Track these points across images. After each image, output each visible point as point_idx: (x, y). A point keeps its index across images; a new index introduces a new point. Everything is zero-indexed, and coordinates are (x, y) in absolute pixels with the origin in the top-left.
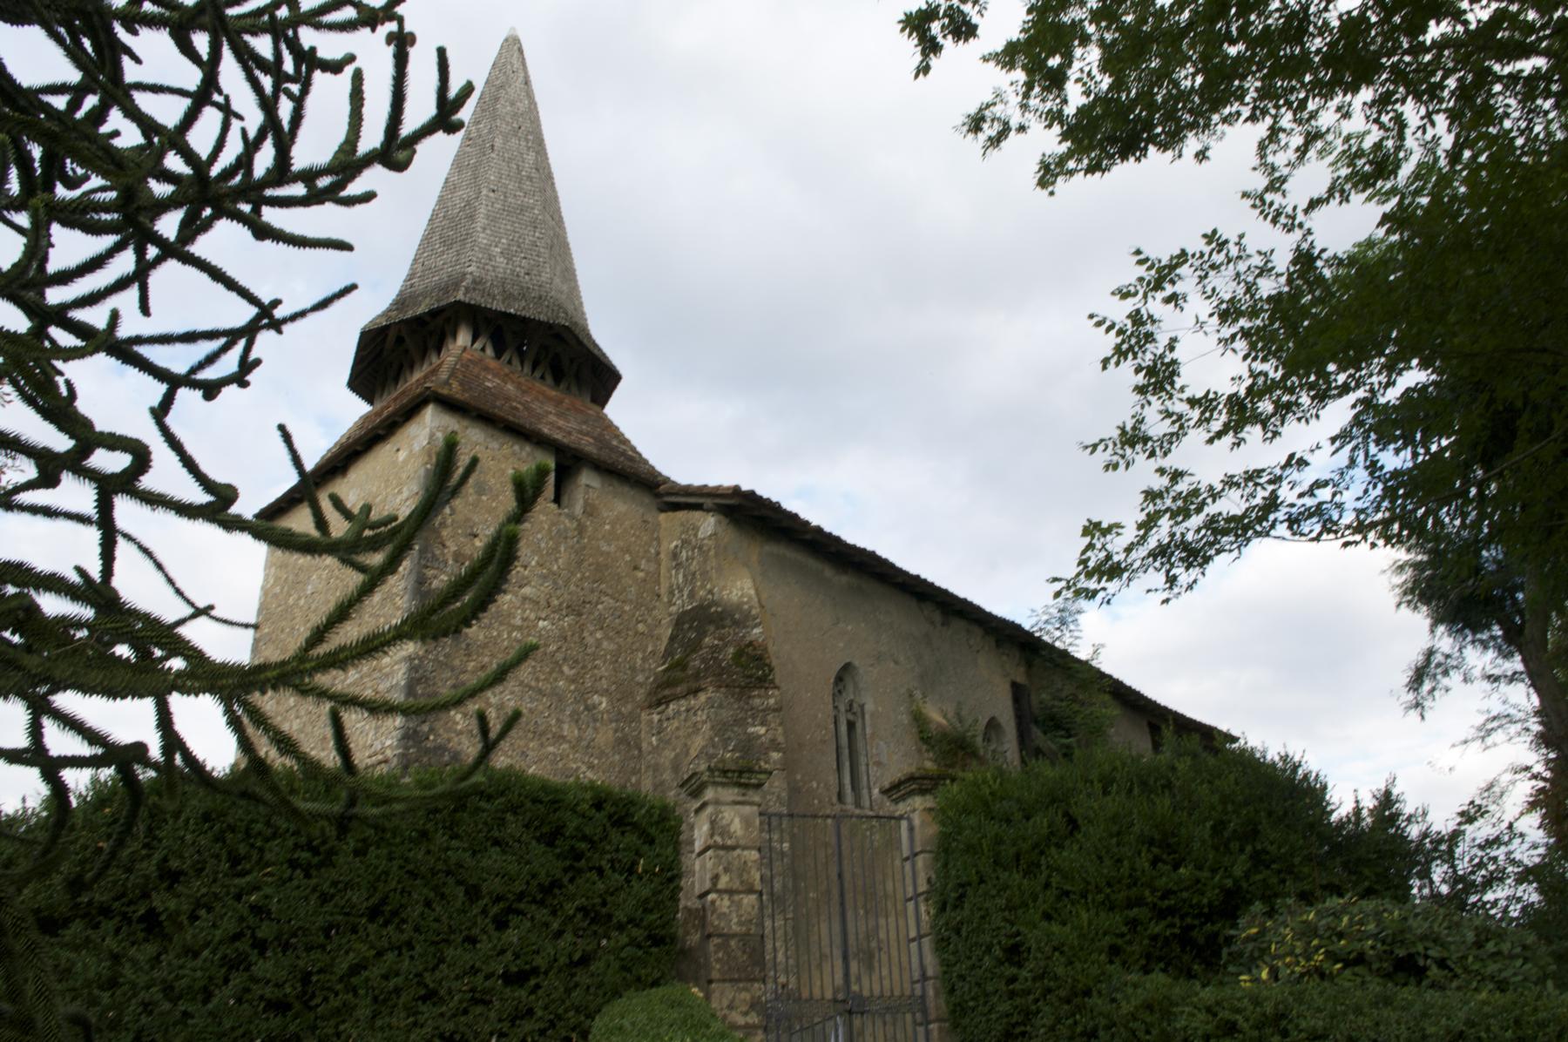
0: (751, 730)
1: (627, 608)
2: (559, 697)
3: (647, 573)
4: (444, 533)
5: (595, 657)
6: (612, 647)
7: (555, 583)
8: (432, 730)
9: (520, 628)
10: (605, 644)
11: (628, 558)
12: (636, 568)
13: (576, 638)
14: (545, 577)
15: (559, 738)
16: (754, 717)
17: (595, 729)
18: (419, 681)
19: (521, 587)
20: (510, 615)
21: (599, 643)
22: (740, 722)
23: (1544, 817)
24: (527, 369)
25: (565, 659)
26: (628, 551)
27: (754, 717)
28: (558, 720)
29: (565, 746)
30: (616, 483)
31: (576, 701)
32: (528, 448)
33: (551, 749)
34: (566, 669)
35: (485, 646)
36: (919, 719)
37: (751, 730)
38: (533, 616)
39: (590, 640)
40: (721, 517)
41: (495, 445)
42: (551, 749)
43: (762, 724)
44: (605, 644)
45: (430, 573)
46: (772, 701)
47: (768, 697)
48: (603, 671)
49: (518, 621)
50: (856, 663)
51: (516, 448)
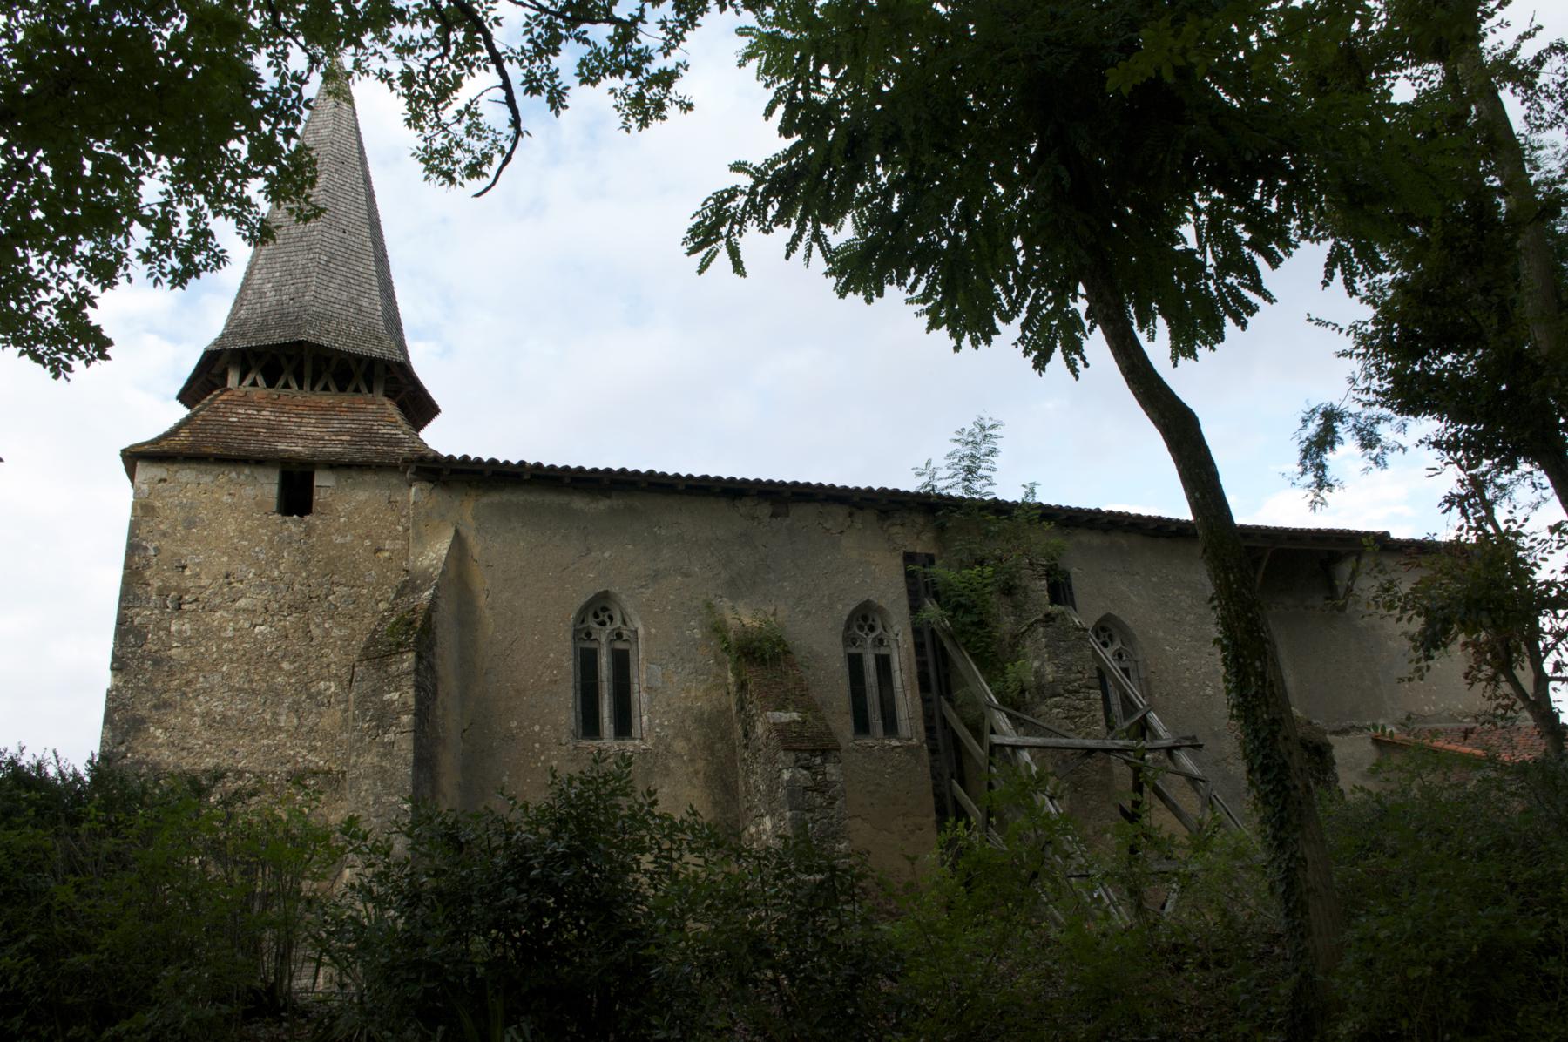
0: (387, 697)
1: (364, 591)
2: (278, 694)
3: (393, 551)
4: (148, 573)
5: (322, 645)
6: (344, 632)
7: (274, 588)
8: (129, 749)
9: (231, 639)
10: (335, 632)
11: (368, 543)
12: (379, 550)
13: (299, 633)
14: (263, 585)
15: (274, 730)
16: (389, 685)
17: (320, 714)
18: (115, 710)
19: (234, 601)
20: (221, 628)
21: (327, 632)
22: (377, 691)
23: (77, 777)
24: (306, 387)
25: (283, 657)
26: (369, 536)
27: (389, 685)
28: (274, 714)
29: (283, 736)
30: (354, 474)
31: (297, 692)
32: (247, 471)
33: (265, 742)
34: (285, 665)
35: (191, 663)
36: (718, 629)
37: (387, 697)
38: (247, 625)
39: (316, 632)
40: (424, 485)
41: (207, 479)
42: (265, 742)
43: (397, 690)
44: (335, 632)
45: (130, 613)
46: (406, 665)
47: (403, 661)
48: (333, 658)
49: (230, 633)
50: (615, 589)
51: (234, 475)
